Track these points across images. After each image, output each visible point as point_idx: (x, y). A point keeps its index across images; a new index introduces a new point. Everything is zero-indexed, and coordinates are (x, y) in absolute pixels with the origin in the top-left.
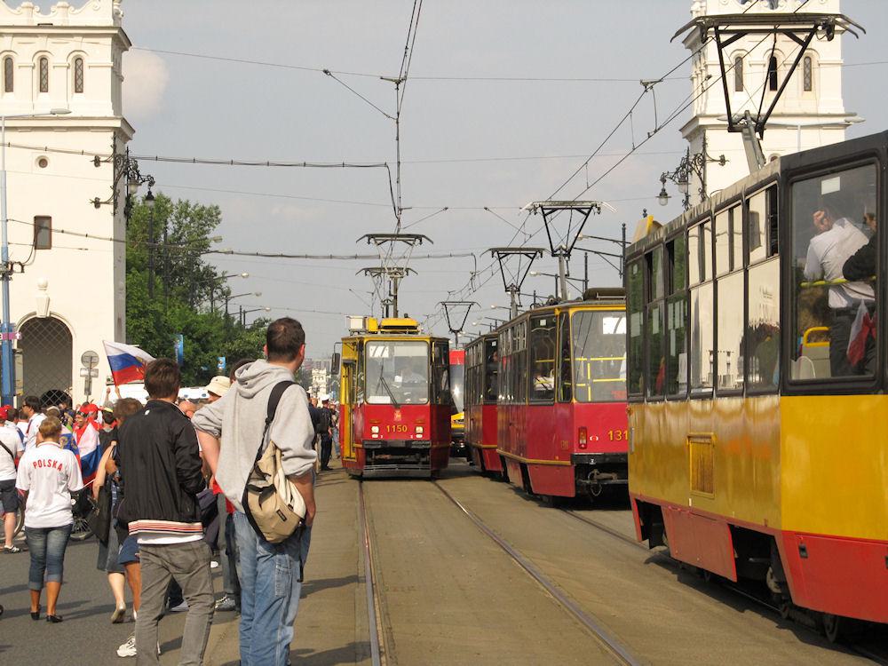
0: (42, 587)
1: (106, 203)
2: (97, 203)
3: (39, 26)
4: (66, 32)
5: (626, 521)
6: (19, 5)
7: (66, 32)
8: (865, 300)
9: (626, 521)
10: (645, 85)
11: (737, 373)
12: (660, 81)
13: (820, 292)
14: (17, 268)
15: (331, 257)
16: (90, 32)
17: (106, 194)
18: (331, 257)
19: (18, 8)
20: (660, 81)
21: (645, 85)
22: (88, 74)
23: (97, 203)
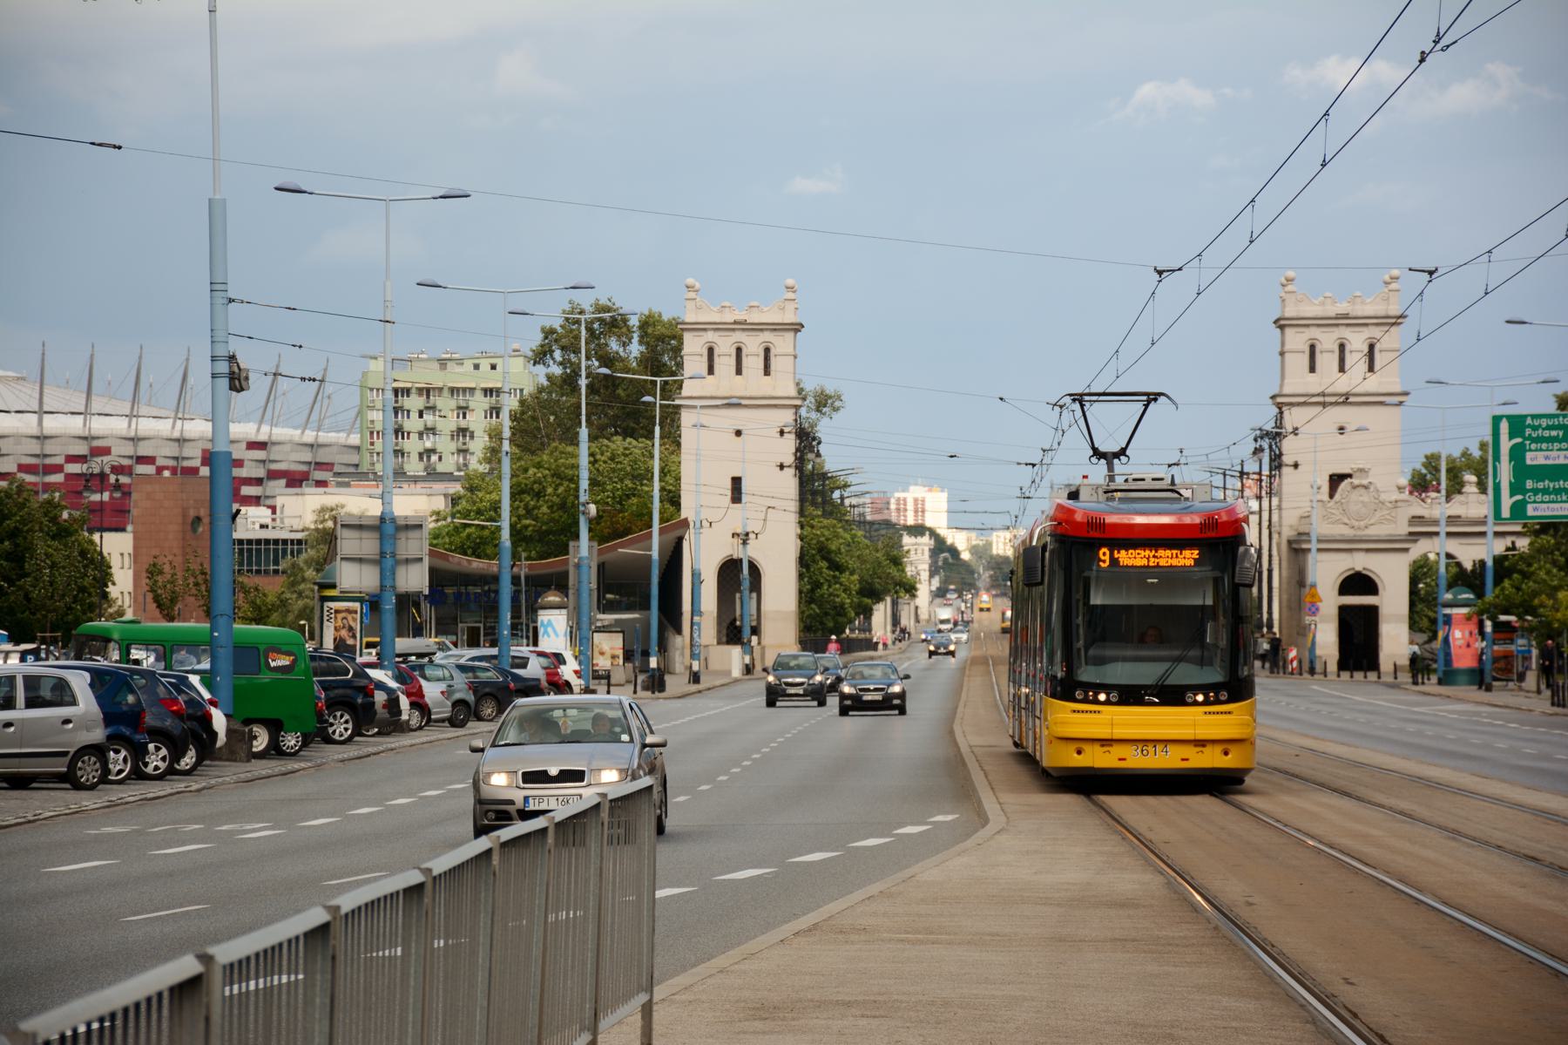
14: (752, 536)
22: (745, 361)
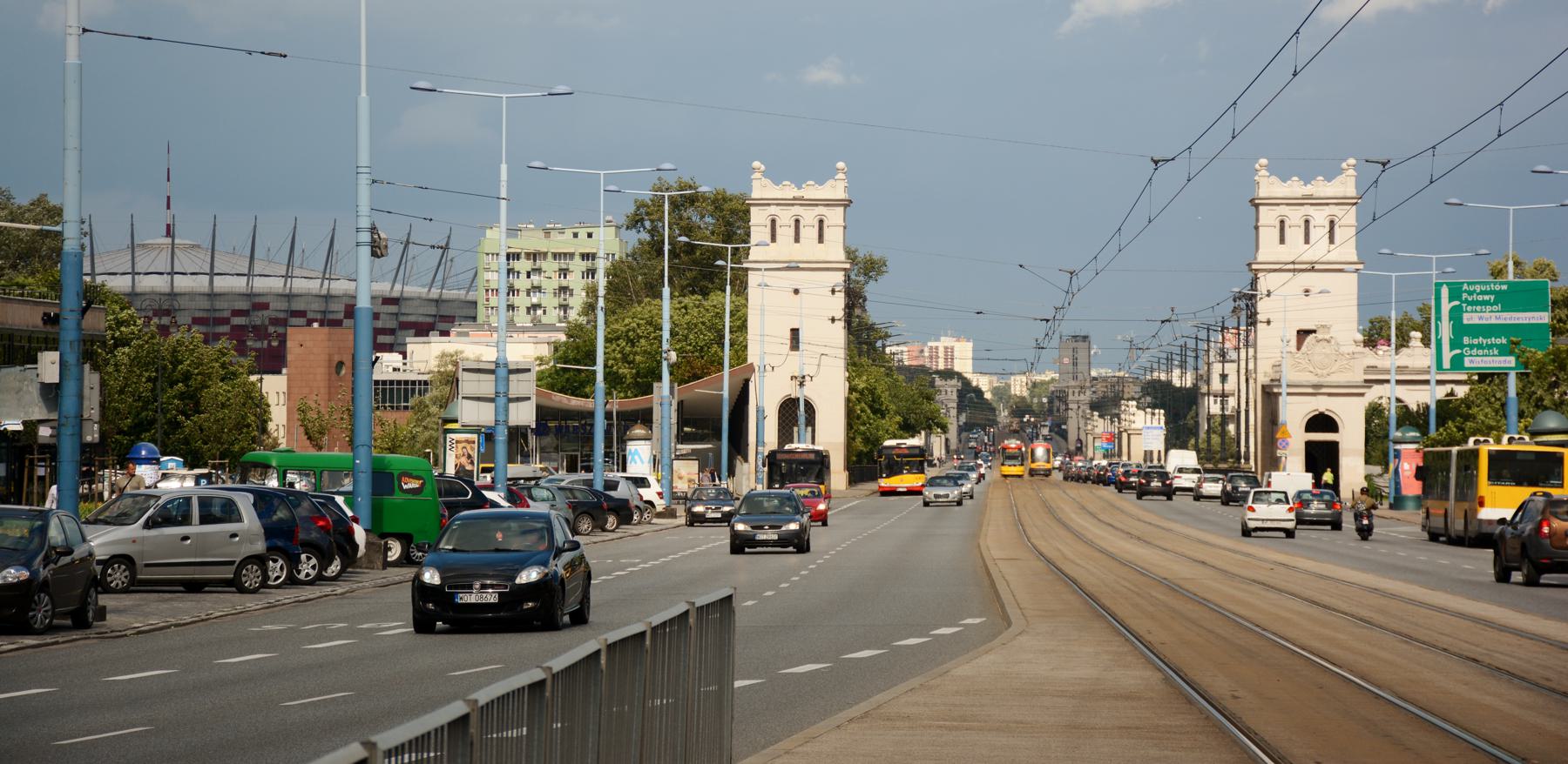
0: (1093, 482)
1: (839, 320)
2: (833, 320)
3: (794, 199)
4: (814, 203)
5: (644, 499)
6: (1289, 179)
7: (814, 203)
8: (594, 372)
9: (644, 499)
10: (1156, 162)
11: (1280, 398)
12: (1173, 159)
13: (553, 369)
15: (826, 346)
16: (830, 203)
17: (840, 314)
18: (826, 346)
19: (1289, 182)
20: (1173, 159)
21: (1156, 162)
22: (803, 231)
23: (833, 320)
